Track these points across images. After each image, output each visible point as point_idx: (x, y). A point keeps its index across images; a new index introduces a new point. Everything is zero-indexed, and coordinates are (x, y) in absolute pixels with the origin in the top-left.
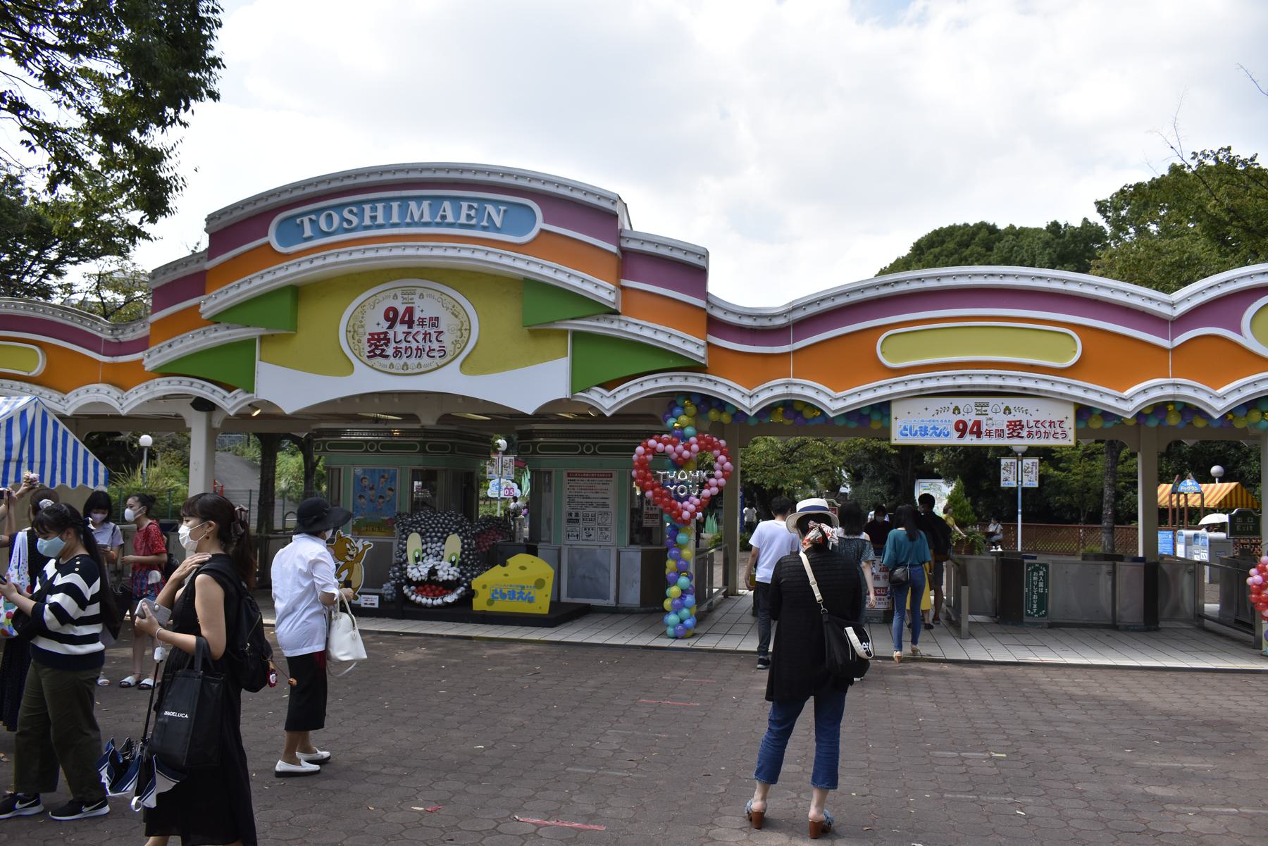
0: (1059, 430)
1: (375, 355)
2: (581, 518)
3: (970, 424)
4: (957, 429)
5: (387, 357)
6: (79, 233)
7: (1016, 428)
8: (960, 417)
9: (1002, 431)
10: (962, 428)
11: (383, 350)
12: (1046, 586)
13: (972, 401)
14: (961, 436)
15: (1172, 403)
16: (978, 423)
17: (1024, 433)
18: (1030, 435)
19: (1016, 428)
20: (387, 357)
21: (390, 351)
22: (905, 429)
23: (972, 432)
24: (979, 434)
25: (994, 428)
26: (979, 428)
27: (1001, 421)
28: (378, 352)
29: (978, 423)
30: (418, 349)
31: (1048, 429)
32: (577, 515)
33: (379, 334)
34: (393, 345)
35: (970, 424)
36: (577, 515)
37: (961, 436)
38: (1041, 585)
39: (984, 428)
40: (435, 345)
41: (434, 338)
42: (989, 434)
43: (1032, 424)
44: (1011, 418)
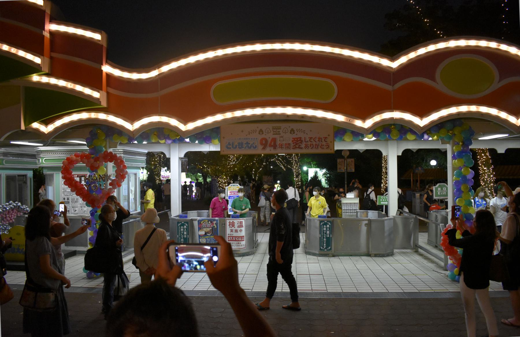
0: (324, 143)
1: (296, 148)
2: (70, 201)
3: (269, 140)
4: (262, 144)
5: (302, 148)
6: (482, 153)
7: (297, 142)
8: (263, 136)
9: (289, 144)
10: (264, 143)
11: (300, 145)
12: (188, 234)
13: (270, 125)
14: (264, 148)
15: (394, 125)
16: (274, 140)
17: (303, 146)
18: (306, 147)
19: (297, 142)
20: (302, 148)
21: (303, 146)
22: (229, 144)
23: (270, 146)
24: (275, 147)
25: (284, 143)
26: (275, 143)
27: (289, 138)
28: (297, 146)
29: (274, 140)
30: (316, 145)
31: (318, 143)
32: (68, 199)
33: (297, 138)
34: (304, 143)
35: (269, 140)
36: (68, 199)
37: (264, 148)
38: (185, 233)
39: (278, 143)
40: (324, 143)
41: (323, 140)
42: (281, 146)
43: (308, 139)
44: (295, 136)
